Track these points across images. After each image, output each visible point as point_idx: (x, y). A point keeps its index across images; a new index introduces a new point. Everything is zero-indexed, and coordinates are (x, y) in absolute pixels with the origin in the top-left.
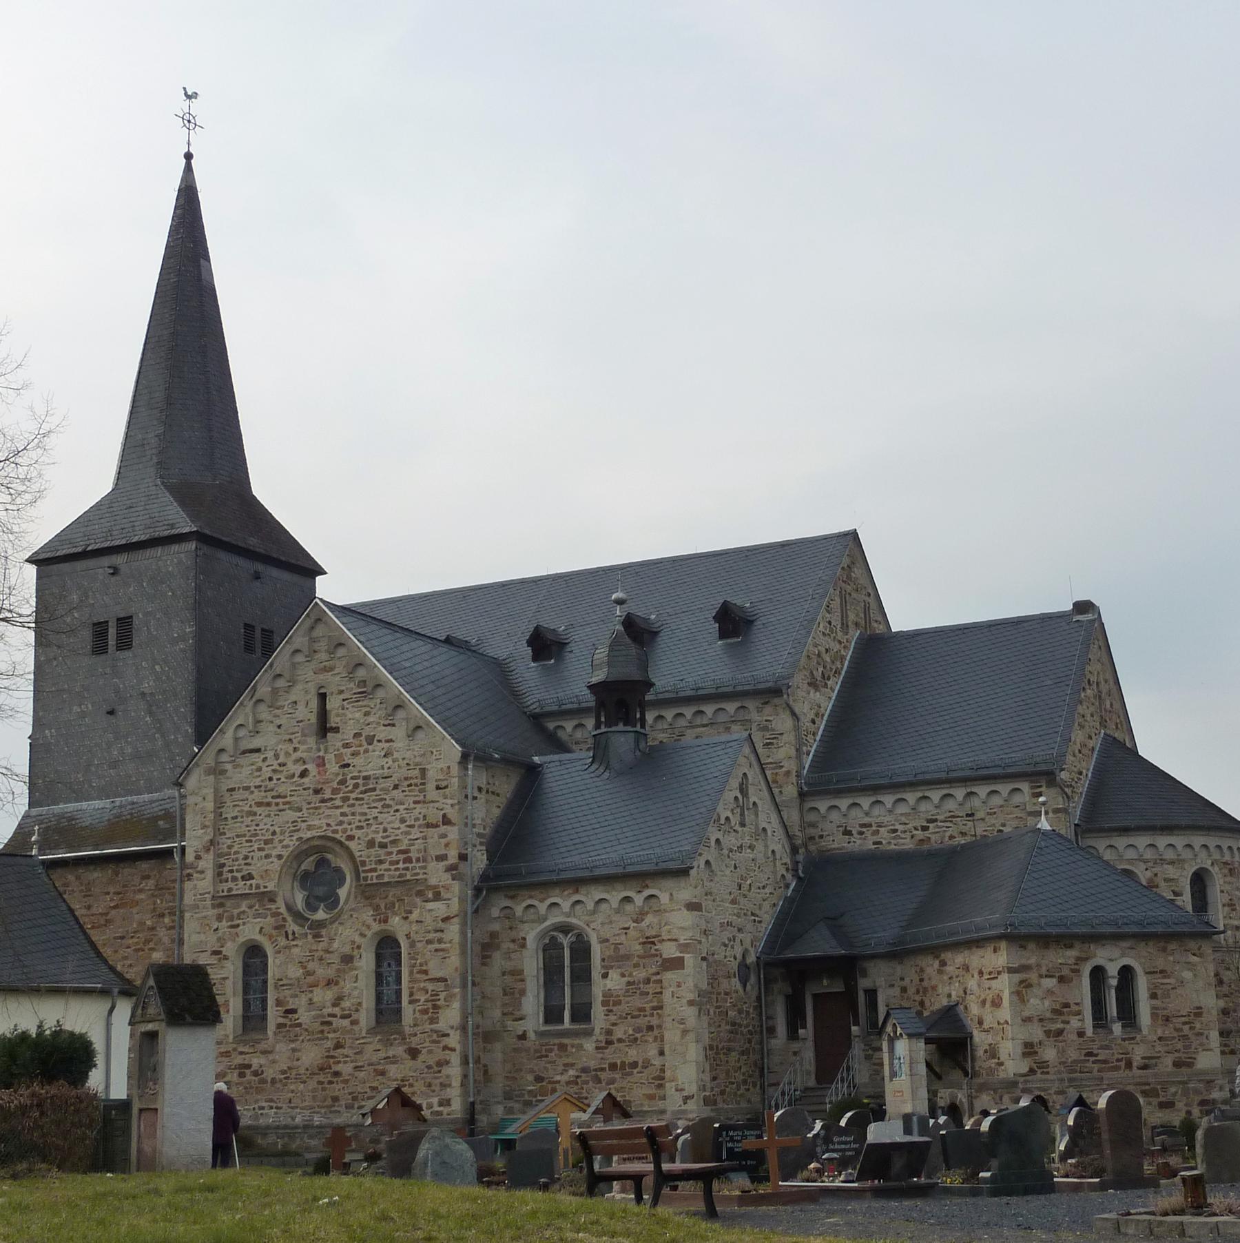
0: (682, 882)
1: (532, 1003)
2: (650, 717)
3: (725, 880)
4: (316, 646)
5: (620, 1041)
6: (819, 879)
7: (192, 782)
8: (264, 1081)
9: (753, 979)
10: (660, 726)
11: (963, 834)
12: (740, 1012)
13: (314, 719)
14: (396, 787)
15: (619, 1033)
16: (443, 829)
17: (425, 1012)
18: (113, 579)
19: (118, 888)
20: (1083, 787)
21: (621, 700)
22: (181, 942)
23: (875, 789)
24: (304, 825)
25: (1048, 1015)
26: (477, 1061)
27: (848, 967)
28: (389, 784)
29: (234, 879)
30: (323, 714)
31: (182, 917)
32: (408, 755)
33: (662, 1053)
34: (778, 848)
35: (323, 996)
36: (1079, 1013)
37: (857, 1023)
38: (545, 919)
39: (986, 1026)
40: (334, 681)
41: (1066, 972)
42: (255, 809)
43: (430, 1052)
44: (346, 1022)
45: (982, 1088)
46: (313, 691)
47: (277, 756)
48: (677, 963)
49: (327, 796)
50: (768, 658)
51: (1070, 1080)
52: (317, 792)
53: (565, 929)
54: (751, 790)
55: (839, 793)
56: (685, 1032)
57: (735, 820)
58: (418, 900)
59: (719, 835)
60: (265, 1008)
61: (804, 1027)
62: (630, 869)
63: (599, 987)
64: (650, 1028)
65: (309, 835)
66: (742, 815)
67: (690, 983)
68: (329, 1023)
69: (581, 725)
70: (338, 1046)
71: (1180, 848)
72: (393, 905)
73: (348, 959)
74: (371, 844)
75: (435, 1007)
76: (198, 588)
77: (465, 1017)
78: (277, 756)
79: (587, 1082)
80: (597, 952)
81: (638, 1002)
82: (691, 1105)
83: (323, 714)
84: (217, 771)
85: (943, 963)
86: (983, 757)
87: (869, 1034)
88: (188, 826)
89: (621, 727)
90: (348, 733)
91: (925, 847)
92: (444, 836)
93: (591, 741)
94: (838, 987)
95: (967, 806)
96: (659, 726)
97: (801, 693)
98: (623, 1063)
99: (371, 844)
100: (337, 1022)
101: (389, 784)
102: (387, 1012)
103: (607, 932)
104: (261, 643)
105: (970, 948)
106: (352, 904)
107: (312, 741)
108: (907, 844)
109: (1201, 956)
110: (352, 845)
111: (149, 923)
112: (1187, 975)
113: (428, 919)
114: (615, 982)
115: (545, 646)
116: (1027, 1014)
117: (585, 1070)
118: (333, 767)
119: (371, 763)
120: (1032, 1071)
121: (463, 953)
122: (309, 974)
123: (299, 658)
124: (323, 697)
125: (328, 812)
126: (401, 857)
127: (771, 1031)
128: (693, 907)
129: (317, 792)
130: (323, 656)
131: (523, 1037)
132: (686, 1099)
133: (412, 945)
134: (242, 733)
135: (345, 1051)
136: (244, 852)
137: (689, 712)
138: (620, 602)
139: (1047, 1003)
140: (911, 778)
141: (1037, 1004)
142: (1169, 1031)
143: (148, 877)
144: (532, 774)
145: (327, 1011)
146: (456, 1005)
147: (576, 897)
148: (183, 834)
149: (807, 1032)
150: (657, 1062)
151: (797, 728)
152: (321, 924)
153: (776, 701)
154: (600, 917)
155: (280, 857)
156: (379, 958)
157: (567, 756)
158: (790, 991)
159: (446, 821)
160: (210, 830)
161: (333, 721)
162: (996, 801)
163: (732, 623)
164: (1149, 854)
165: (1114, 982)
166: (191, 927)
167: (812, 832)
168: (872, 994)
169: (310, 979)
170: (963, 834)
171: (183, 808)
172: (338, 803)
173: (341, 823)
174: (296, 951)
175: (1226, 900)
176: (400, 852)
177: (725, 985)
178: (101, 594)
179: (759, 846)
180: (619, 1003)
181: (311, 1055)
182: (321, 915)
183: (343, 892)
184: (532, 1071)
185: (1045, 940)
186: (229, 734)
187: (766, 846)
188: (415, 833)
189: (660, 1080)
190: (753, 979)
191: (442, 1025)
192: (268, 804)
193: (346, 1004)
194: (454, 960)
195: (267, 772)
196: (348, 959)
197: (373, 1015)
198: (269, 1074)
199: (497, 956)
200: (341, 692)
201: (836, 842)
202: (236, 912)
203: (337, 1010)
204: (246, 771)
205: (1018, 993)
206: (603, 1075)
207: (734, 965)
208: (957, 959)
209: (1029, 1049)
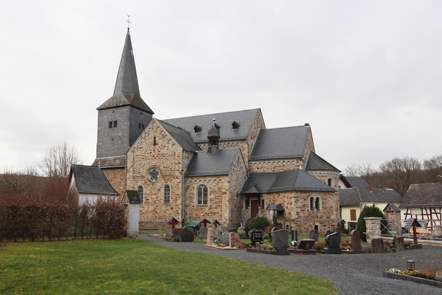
1: (195, 200)
3: (235, 177)
6: (251, 177)
7: (128, 154)
9: (239, 197)
13: (153, 142)
15: (213, 206)
16: (179, 165)
23: (264, 160)
27: (259, 195)
28: (168, 155)
30: (155, 141)
32: (172, 150)
34: (244, 171)
35: (154, 197)
40: (157, 135)
41: (305, 198)
44: (158, 202)
45: (287, 221)
48: (225, 193)
52: (153, 156)
53: (203, 185)
55: (257, 160)
56: (226, 207)
57: (237, 165)
63: (209, 197)
64: (219, 206)
67: (228, 197)
70: (157, 207)
73: (159, 190)
74: (164, 167)
76: (130, 116)
77: (182, 202)
80: (209, 190)
83: (155, 141)
85: (279, 195)
90: (160, 145)
94: (256, 199)
99: (164, 167)
101: (168, 155)
102: (167, 201)
103: (211, 186)
107: (153, 146)
108: (270, 171)
110: (160, 167)
112: (330, 200)
113: (175, 182)
114: (212, 196)
115: (197, 129)
117: (206, 213)
118: (157, 152)
119: (164, 151)
120: (298, 218)
121: (182, 189)
122: (151, 192)
123: (150, 130)
124: (155, 138)
127: (242, 207)
128: (229, 182)
129: (153, 156)
130: (155, 129)
131: (193, 206)
132: (226, 220)
133: (172, 187)
134: (139, 144)
137: (227, 143)
141: (299, 204)
142: (326, 211)
144: (196, 154)
146: (181, 199)
149: (250, 208)
151: (248, 147)
152: (154, 183)
153: (245, 142)
156: (165, 190)
159: (179, 163)
161: (157, 142)
162: (289, 163)
163: (235, 126)
164: (320, 175)
165: (315, 200)
167: (251, 168)
168: (263, 201)
178: (109, 116)
179: (241, 170)
181: (151, 208)
182: (154, 181)
183: (158, 176)
185: (302, 192)
186: (136, 145)
188: (173, 165)
190: (239, 197)
193: (159, 198)
194: (180, 191)
195: (143, 152)
196: (159, 190)
198: (143, 212)
199: (188, 190)
201: (255, 170)
204: (140, 152)
206: (210, 215)
207: (236, 194)
209: (298, 213)
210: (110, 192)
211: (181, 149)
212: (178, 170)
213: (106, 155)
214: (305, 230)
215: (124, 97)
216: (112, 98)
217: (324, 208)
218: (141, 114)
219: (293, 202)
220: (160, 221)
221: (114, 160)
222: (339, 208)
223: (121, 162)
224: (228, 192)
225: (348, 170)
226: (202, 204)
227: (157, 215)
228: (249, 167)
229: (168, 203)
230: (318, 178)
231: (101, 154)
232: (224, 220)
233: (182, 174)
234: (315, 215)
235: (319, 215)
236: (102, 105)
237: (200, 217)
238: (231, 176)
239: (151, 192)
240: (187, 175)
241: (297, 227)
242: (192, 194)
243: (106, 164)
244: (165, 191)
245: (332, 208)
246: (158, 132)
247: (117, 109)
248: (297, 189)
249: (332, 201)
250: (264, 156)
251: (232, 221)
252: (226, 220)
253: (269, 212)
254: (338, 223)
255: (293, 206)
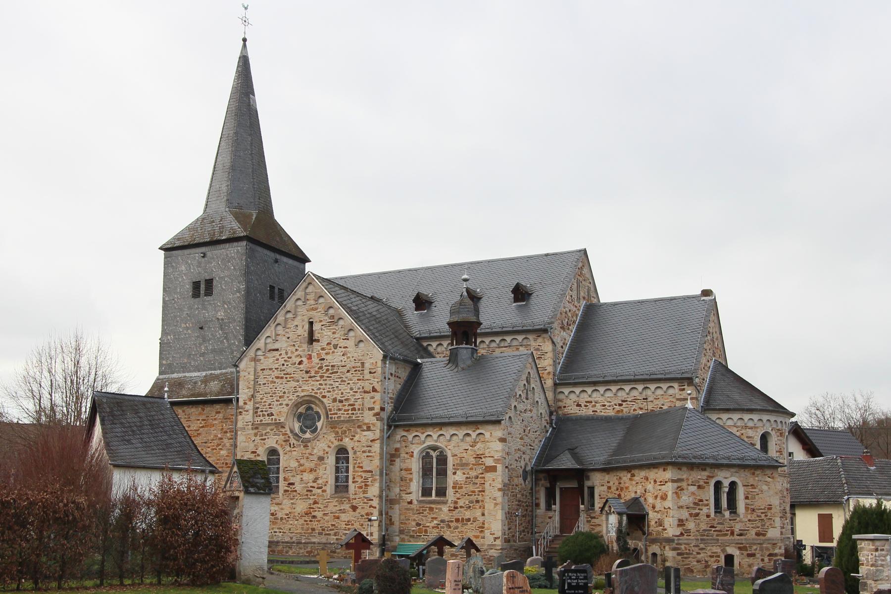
0: (497, 427)
1: (415, 486)
2: (479, 340)
3: (517, 427)
4: (308, 297)
5: (461, 507)
6: (561, 428)
7: (242, 365)
8: (276, 519)
9: (529, 479)
10: (482, 346)
11: (641, 409)
12: (523, 495)
13: (306, 335)
14: (348, 371)
15: (461, 503)
16: (373, 394)
17: (361, 487)
18: (203, 260)
19: (204, 417)
20: (705, 387)
21: (465, 331)
22: (236, 446)
23: (595, 383)
24: (300, 389)
25: (692, 505)
26: (387, 514)
27: (580, 474)
28: (345, 370)
29: (264, 415)
30: (311, 332)
31: (236, 434)
33: (483, 515)
34: (543, 411)
36: (707, 505)
37: (583, 504)
38: (424, 442)
39: (657, 509)
40: (317, 316)
41: (701, 483)
42: (275, 380)
43: (363, 508)
44: (320, 491)
45: (654, 541)
46: (306, 320)
47: (287, 353)
48: (493, 469)
49: (313, 374)
50: (540, 311)
51: (702, 540)
52: (307, 372)
53: (434, 448)
54: (532, 381)
55: (575, 384)
56: (496, 504)
57: (524, 396)
58: (358, 430)
59: (516, 403)
60: (278, 482)
61: (555, 504)
62: (470, 419)
63: (451, 479)
64: (477, 501)
65: (303, 394)
66: (527, 393)
67: (500, 480)
68: (311, 491)
69: (441, 344)
70: (315, 503)
71: (756, 421)
72: (345, 432)
73: (321, 459)
74: (335, 400)
75: (366, 485)
76: (247, 266)
77: (381, 491)
78: (287, 353)
79: (443, 527)
80: (450, 461)
81: (471, 488)
82: (498, 542)
83: (311, 332)
84: (255, 360)
85: (633, 475)
86: (654, 369)
87: (589, 510)
88: (240, 387)
89: (464, 346)
91: (620, 414)
92: (373, 398)
93: (448, 353)
94: (574, 485)
95: (644, 393)
96: (484, 347)
97: (557, 332)
98: (463, 519)
99: (335, 400)
100: (315, 491)
101: (345, 370)
102: (341, 487)
103: (457, 451)
104: (278, 296)
105: (649, 468)
106: (324, 431)
107: (305, 346)
108: (611, 413)
109: (773, 478)
110: (325, 400)
111: (219, 436)
112: (765, 488)
113: (363, 439)
114: (460, 477)
115: (422, 303)
116: (680, 504)
117: (442, 521)
118: (315, 360)
119: (335, 358)
120: (682, 534)
121: (381, 458)
122: (301, 465)
123: (300, 303)
124: (311, 324)
125: (313, 383)
126: (350, 407)
127: (538, 505)
128: (503, 440)
129: (307, 372)
130: (312, 302)
131: (410, 503)
132: (495, 539)
133: (355, 453)
134: (269, 340)
135: (319, 506)
136: (269, 401)
137: (497, 339)
138: (466, 280)
139: (691, 499)
140: (615, 378)
141: (686, 499)
142: (754, 517)
143: (219, 412)
144: (417, 367)
145: (309, 485)
146: (377, 485)
147: (441, 432)
148: (238, 392)
149: (557, 507)
150: (481, 519)
151: (554, 350)
152: (309, 440)
153: (544, 335)
154: (454, 444)
155: (287, 405)
156: (338, 460)
157: (432, 359)
158: (548, 485)
159: (374, 390)
160: (252, 390)
161: (316, 336)
163: (521, 294)
164: (739, 423)
165: (727, 490)
166: (241, 438)
167: (560, 404)
168: (592, 489)
169: (302, 468)
170: (641, 409)
171: (238, 379)
172: (318, 378)
173: (319, 389)
174: (294, 453)
175: (778, 449)
176: (349, 405)
177: (516, 481)
178: (192, 266)
179: (534, 410)
180: (461, 488)
181: (301, 507)
182: (308, 435)
183: (319, 425)
184: (414, 520)
185: (692, 466)
186: (262, 341)
187: (538, 410)
188: (358, 396)
189: (482, 528)
190: (529, 479)
191: (369, 495)
192: (282, 378)
193: (320, 481)
194: (377, 462)
195: (281, 361)
196: (321, 459)
197: (334, 487)
198: (279, 515)
199: (398, 460)
200: (321, 321)
201: (572, 410)
202: (264, 432)
203: (315, 485)
204: (271, 360)
205: (676, 493)
206: (452, 524)
207: (521, 471)
208: (640, 474)
209: (681, 523)
210: (194, 463)
211: (379, 354)
212: (371, 409)
213: (185, 369)
214: (699, 567)
215: (230, 218)
216: (202, 220)
217: (750, 509)
218: (276, 261)
219: (670, 494)
220: (324, 540)
221: (206, 380)
222: (788, 509)
223: (223, 386)
224: (500, 467)
225: (813, 410)
226: (434, 497)
227: (314, 524)
228: (557, 400)
229: (344, 495)
230: (734, 430)
231: (170, 366)
232: (489, 539)
233: (381, 420)
234: (726, 526)
235: (737, 528)
236: (174, 238)
237: (426, 531)
238: (508, 424)
239: (301, 465)
240: (394, 420)
241: (680, 557)
242: (406, 470)
243: (184, 392)
244: (337, 462)
245: (770, 509)
246: (321, 309)
247: (213, 247)
248: (680, 460)
249: (772, 492)
250: (595, 372)
251: (509, 541)
252: (495, 539)
253: (607, 519)
254: (786, 550)
255: (668, 503)
